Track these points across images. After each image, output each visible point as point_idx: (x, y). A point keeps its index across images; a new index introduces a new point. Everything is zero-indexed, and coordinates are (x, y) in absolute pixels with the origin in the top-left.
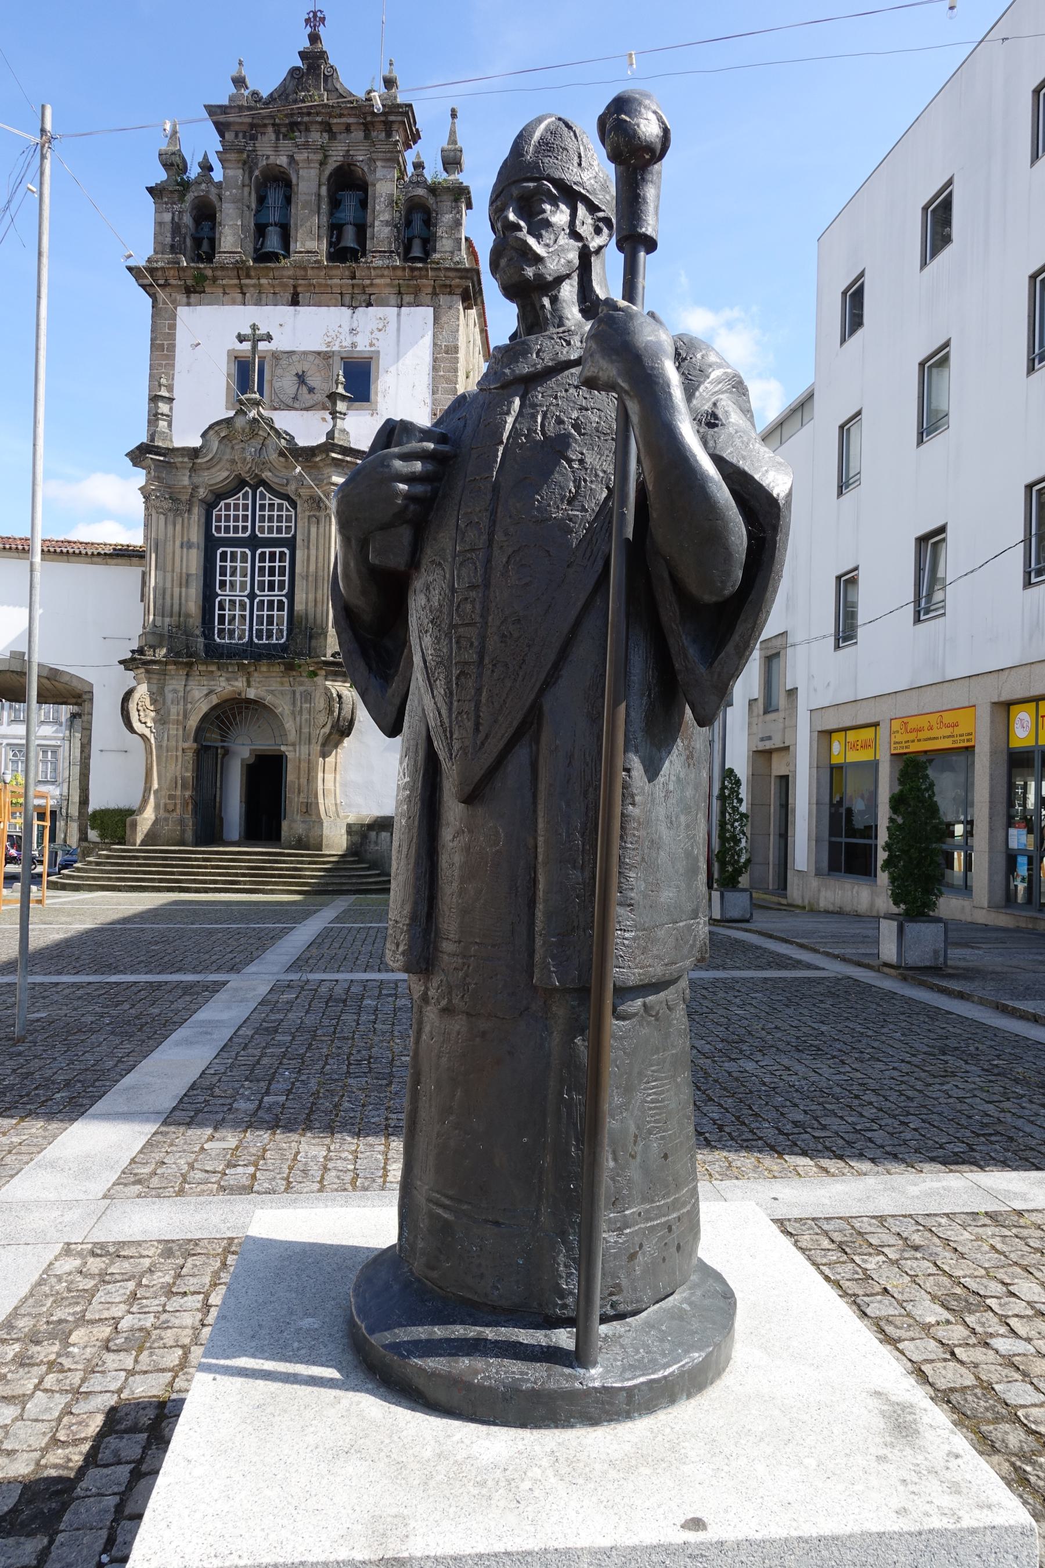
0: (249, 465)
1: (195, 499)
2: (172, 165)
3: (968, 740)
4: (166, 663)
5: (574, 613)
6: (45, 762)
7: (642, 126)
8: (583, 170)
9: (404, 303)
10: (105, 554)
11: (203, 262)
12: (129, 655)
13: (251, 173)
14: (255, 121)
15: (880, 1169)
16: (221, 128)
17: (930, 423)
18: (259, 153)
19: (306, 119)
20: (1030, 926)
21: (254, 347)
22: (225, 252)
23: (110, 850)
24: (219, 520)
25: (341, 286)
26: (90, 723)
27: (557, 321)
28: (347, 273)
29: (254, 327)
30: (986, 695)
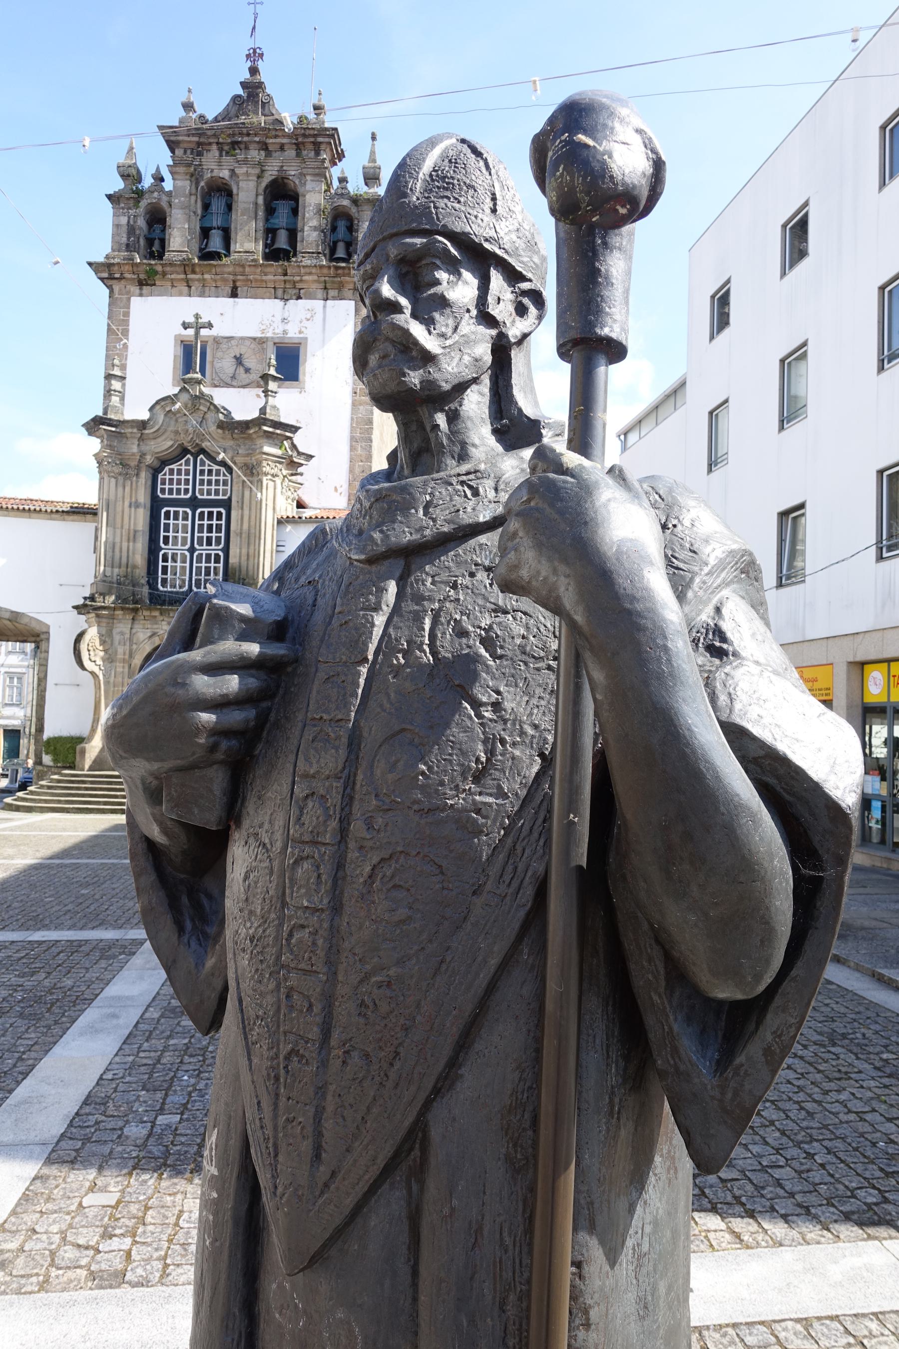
0: (191, 436)
1: (142, 465)
2: (129, 176)
3: (826, 695)
4: (114, 609)
5: (483, 979)
6: (11, 687)
7: (616, 155)
8: (499, 219)
9: (329, 296)
10: (63, 511)
11: (154, 259)
12: (81, 602)
13: (197, 184)
14: (202, 140)
15: (794, 1233)
16: (172, 145)
17: (790, 411)
18: (205, 167)
19: (246, 139)
20: (885, 866)
21: (197, 334)
22: (173, 251)
23: (62, 775)
24: (163, 483)
25: (275, 282)
26: (47, 660)
27: (457, 449)
28: (280, 270)
29: (197, 316)
30: (842, 656)
